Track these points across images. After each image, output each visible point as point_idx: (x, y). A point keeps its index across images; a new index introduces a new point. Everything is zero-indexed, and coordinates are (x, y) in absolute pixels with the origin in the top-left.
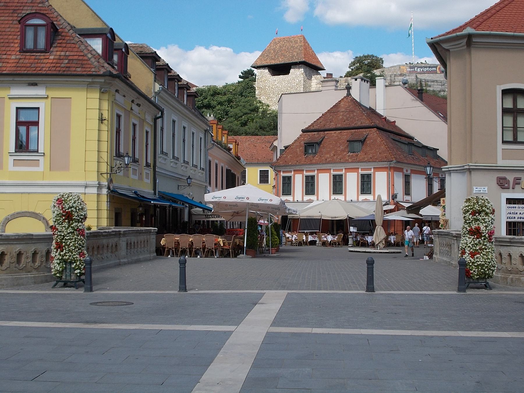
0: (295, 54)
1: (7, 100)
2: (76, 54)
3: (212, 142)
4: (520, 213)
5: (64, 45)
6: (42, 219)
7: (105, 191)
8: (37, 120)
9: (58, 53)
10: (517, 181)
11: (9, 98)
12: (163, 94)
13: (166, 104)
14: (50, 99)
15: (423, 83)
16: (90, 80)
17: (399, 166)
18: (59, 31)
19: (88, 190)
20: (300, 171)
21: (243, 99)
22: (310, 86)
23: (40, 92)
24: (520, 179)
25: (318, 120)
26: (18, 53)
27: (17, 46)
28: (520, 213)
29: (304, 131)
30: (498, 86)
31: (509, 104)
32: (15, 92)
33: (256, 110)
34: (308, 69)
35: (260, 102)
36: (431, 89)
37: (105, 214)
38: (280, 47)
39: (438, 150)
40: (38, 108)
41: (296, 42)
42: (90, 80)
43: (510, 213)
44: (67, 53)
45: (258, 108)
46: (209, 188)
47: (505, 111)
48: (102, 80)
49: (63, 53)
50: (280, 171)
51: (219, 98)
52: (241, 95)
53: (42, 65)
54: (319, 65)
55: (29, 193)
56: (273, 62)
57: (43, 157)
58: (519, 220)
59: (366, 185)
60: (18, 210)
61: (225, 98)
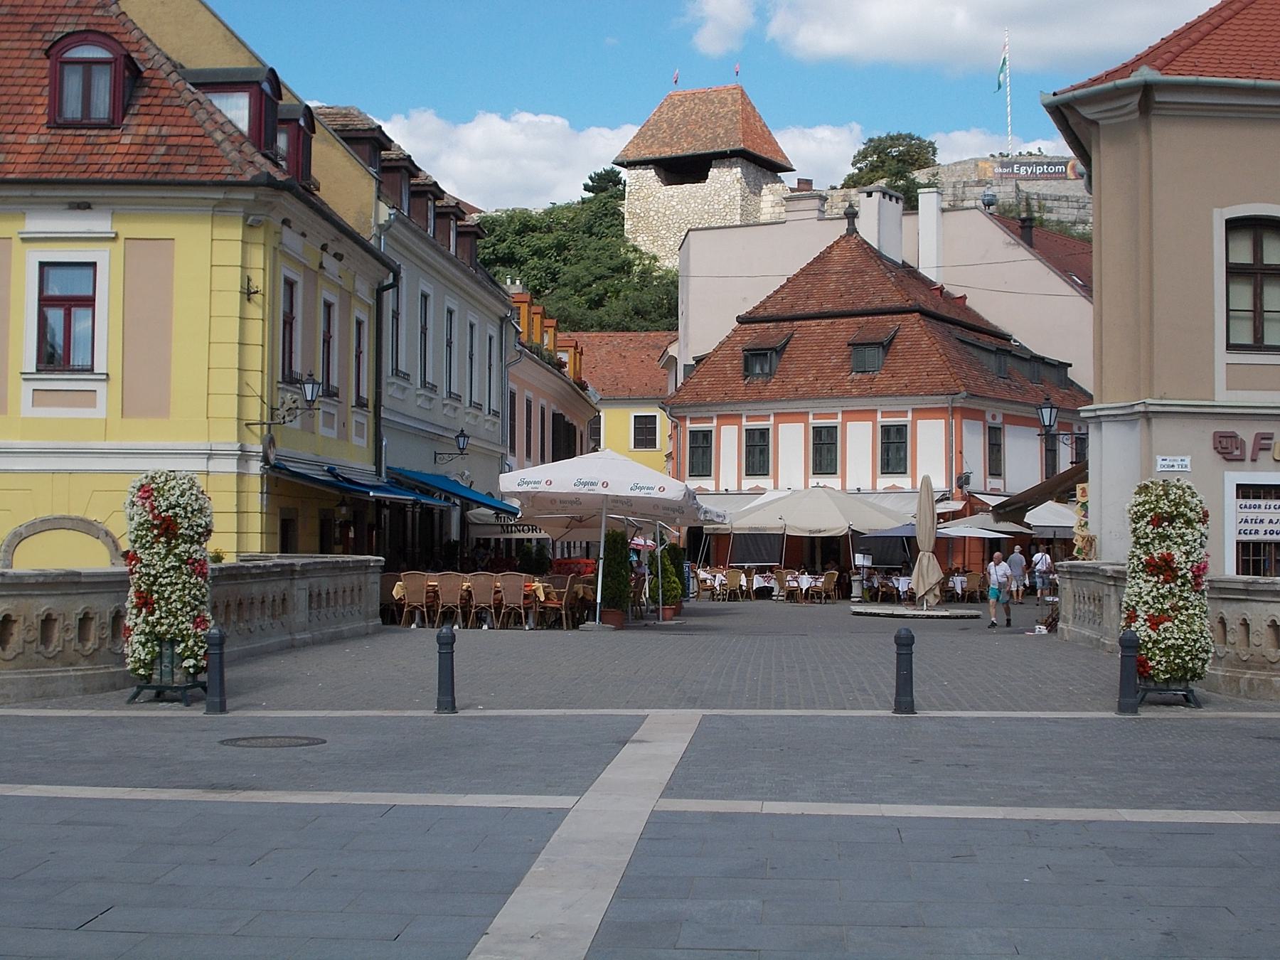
0: (721, 131)
1: (16, 244)
2: (185, 131)
3: (519, 348)
4: (1271, 521)
5: (157, 110)
6: (102, 535)
7: (256, 467)
8: (91, 293)
9: (142, 130)
10: (1263, 443)
11: (23, 239)
12: (399, 230)
13: (406, 253)
14: (121, 242)
15: (1034, 203)
16: (219, 195)
17: (974, 404)
18: (145, 75)
19: (215, 465)
20: (734, 418)
21: (594, 242)
22: (758, 210)
23: (99, 224)
24: (1269, 437)
25: (776, 292)
26: (44, 130)
27: (41, 112)
28: (1271, 521)
29: (742, 320)
30: (1216, 211)
31: (1243, 255)
32: (38, 224)
33: (625, 267)
34: (752, 167)
35: (636, 250)
36: (1054, 217)
37: (255, 523)
38: (685, 114)
39: (1070, 365)
40: (94, 265)
41: (723, 103)
42: (220, 196)
43: (1246, 521)
44: (165, 131)
45: (630, 264)
46: (511, 460)
47: (1234, 272)
48: (249, 195)
49: (153, 130)
50: (683, 419)
51: (536, 240)
52: (589, 231)
53: (104, 159)
54: (779, 160)
55: (71, 472)
56: (667, 152)
57: (104, 384)
58: (1268, 537)
59: (894, 451)
60: (45, 514)
61: (549, 239)
